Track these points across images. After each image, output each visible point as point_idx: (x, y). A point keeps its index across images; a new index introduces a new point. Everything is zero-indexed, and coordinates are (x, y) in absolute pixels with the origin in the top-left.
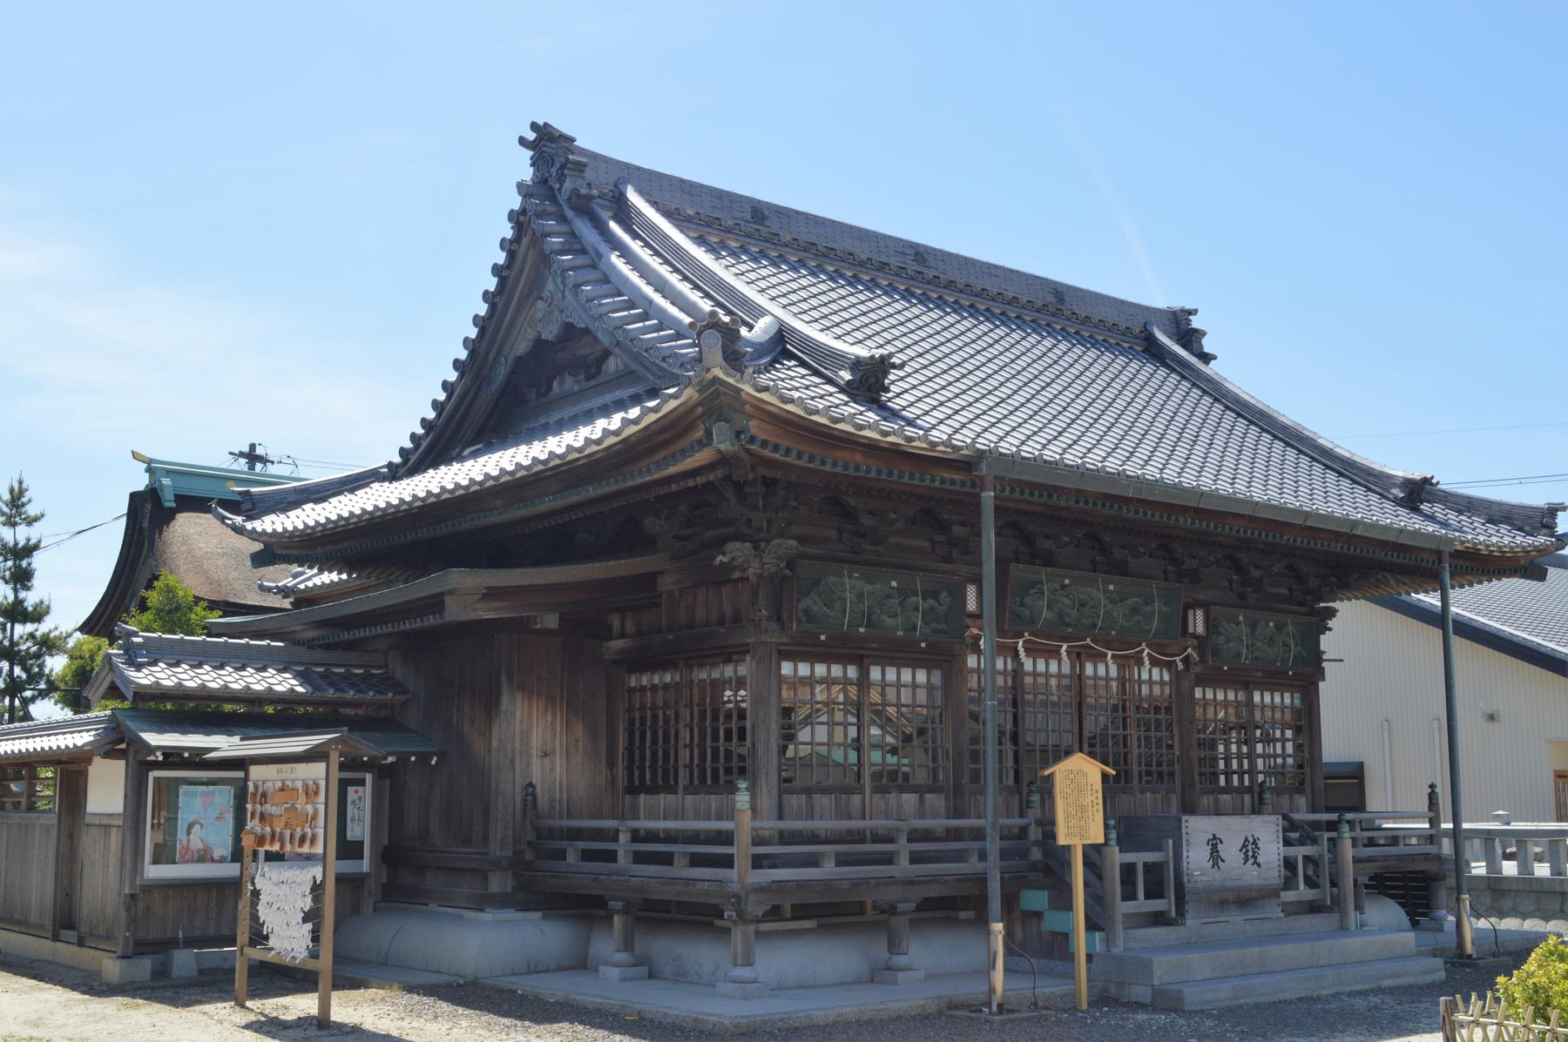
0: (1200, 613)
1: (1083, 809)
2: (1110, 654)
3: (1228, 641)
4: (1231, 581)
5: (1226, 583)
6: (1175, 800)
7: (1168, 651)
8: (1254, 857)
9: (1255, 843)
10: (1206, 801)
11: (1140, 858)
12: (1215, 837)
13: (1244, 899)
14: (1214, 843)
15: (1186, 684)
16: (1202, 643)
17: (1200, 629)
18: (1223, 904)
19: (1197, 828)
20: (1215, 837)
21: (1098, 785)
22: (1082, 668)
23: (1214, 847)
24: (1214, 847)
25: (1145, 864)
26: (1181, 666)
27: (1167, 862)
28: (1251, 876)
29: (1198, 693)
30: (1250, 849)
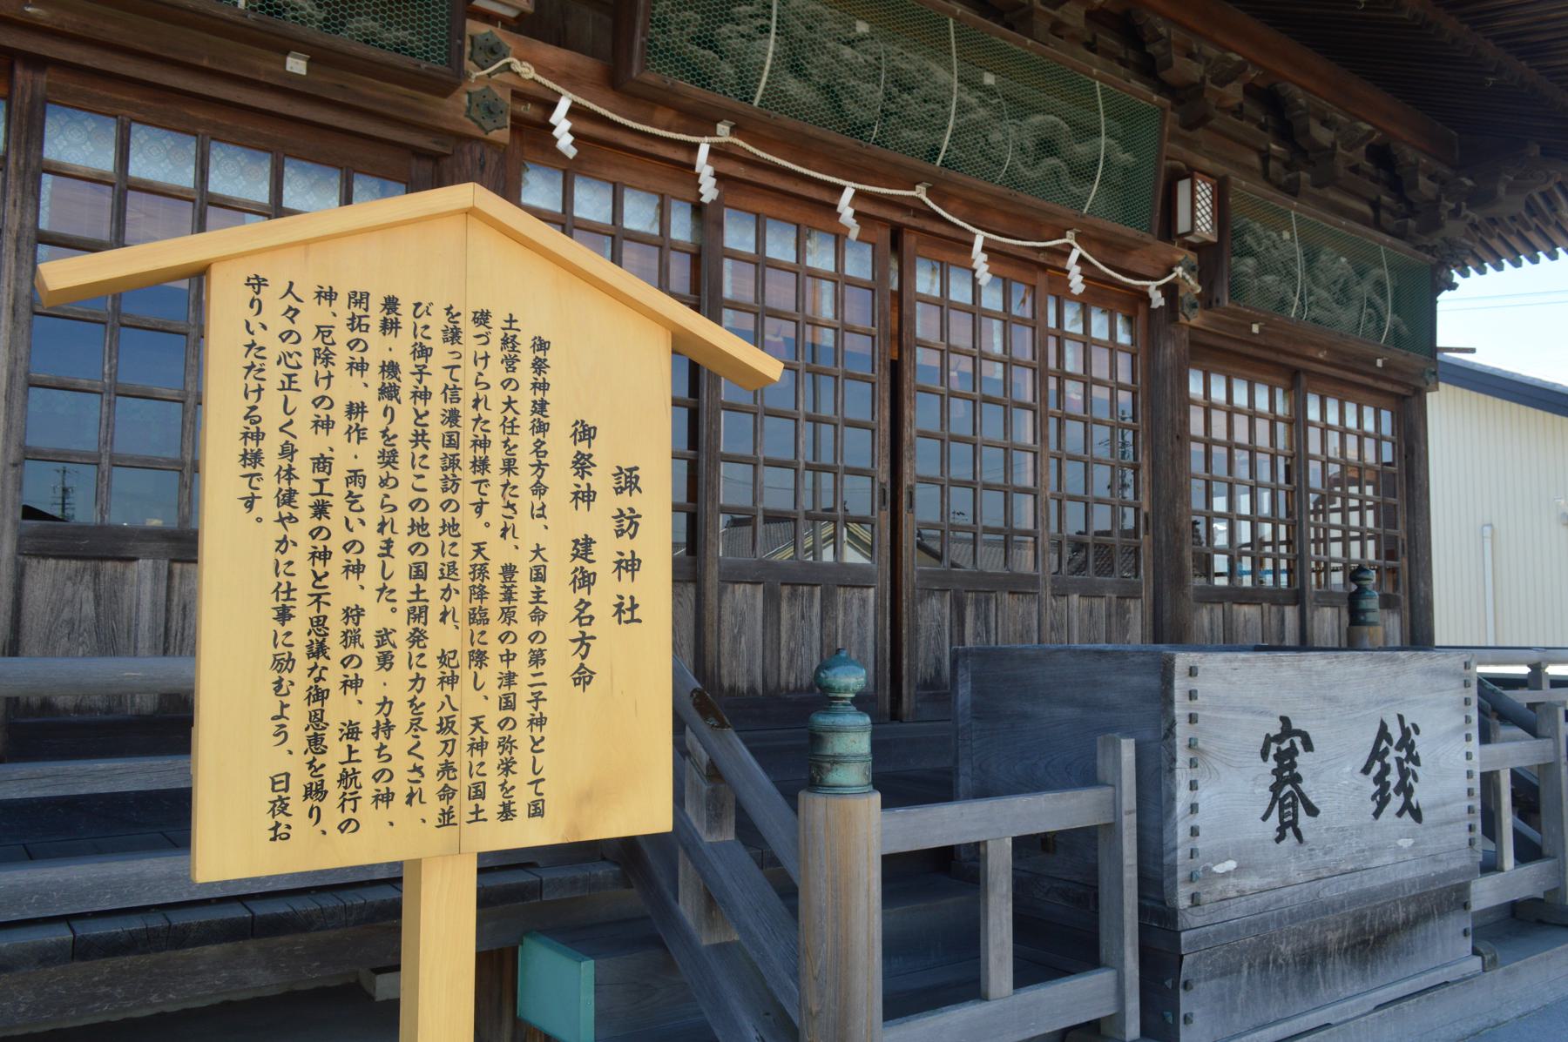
0: (1204, 191)
1: (492, 594)
2: (979, 240)
3: (1263, 269)
4: (1265, 156)
5: (1255, 160)
6: (1137, 612)
7: (1128, 263)
8: (1405, 789)
9: (1406, 743)
10: (1206, 618)
11: (990, 823)
12: (1287, 729)
13: (1372, 935)
14: (1286, 748)
15: (1168, 351)
16: (1209, 259)
17: (1205, 226)
18: (1310, 961)
19: (1229, 695)
20: (1287, 729)
21: (646, 437)
22: (906, 275)
23: (1286, 761)
24: (1286, 761)
25: (1022, 844)
26: (1158, 300)
27: (1112, 829)
28: (1399, 854)
29: (1195, 387)
30: (1392, 762)
